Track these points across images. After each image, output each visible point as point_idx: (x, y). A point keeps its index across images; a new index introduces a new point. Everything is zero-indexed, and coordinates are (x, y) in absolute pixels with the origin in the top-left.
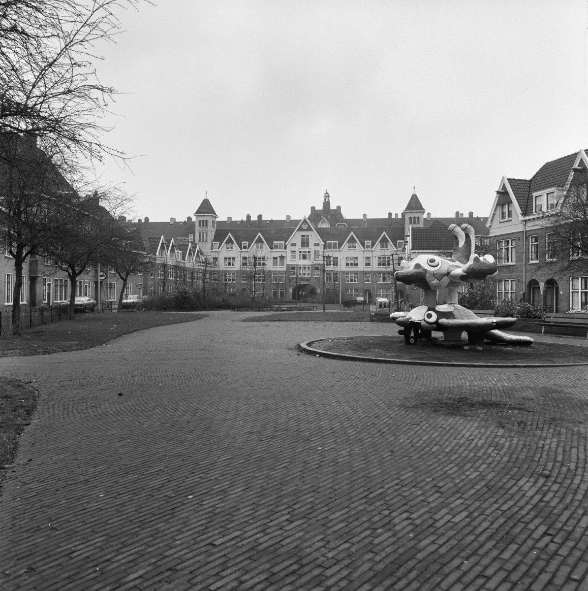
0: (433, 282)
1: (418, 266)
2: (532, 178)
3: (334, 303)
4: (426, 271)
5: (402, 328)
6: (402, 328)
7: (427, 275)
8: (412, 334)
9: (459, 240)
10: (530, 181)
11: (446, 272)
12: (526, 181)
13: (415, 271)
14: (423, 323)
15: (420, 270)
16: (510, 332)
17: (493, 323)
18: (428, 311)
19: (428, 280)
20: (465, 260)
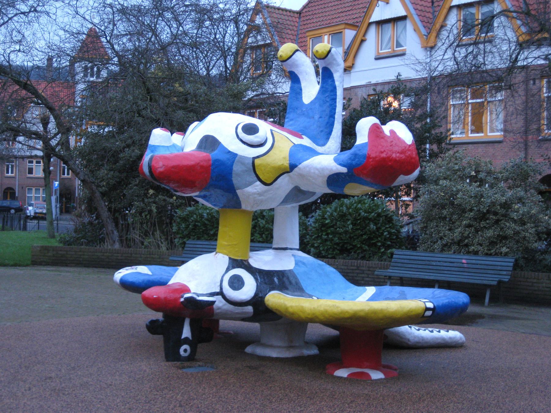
0: (250, 189)
1: (209, 142)
2: (304, 7)
3: (252, 236)
4: (234, 155)
5: (159, 316)
6: (159, 316)
7: (237, 168)
8: (186, 333)
9: (303, 84)
10: (299, 13)
11: (286, 163)
12: (290, 11)
13: (203, 154)
14: (219, 302)
15: (215, 155)
16: (433, 325)
17: (427, 309)
18: (228, 270)
19: (236, 181)
20: (153, 163)
